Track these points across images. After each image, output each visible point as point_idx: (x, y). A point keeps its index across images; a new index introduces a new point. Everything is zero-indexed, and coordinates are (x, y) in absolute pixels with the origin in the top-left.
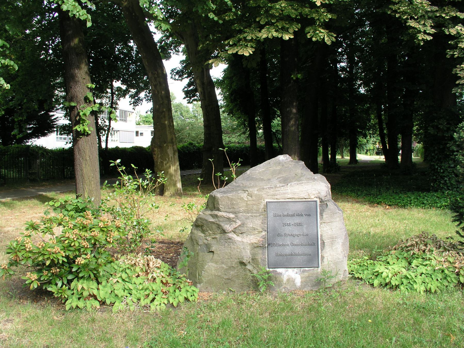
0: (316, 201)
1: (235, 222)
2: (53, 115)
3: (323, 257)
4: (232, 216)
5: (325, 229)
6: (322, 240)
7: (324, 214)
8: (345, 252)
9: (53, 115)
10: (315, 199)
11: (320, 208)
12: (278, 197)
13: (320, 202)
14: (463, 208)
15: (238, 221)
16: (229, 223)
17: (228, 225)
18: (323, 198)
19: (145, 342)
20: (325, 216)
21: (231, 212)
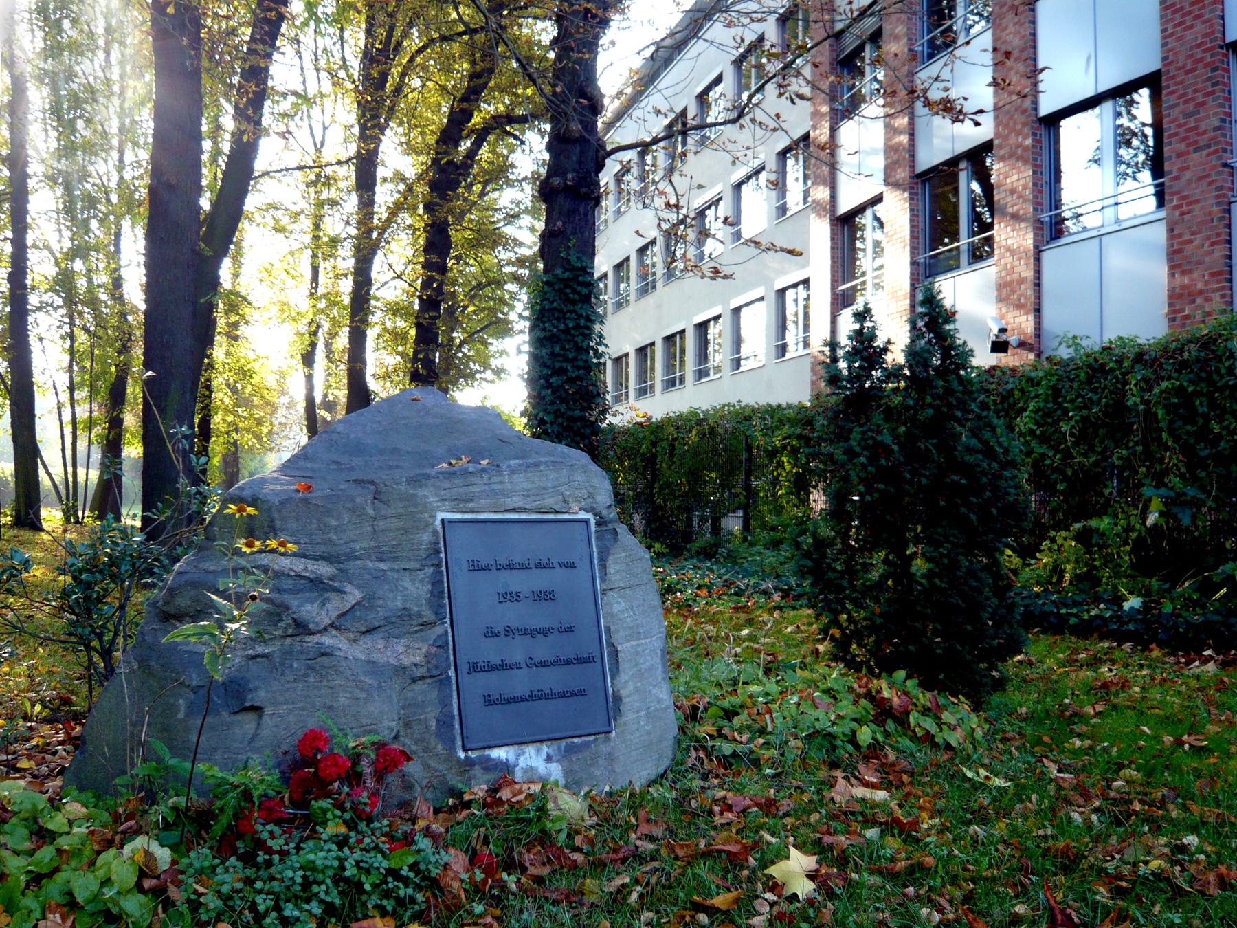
0: (586, 521)
4: (324, 569)
10: (582, 515)
13: (598, 524)
17: (316, 605)
18: (605, 513)
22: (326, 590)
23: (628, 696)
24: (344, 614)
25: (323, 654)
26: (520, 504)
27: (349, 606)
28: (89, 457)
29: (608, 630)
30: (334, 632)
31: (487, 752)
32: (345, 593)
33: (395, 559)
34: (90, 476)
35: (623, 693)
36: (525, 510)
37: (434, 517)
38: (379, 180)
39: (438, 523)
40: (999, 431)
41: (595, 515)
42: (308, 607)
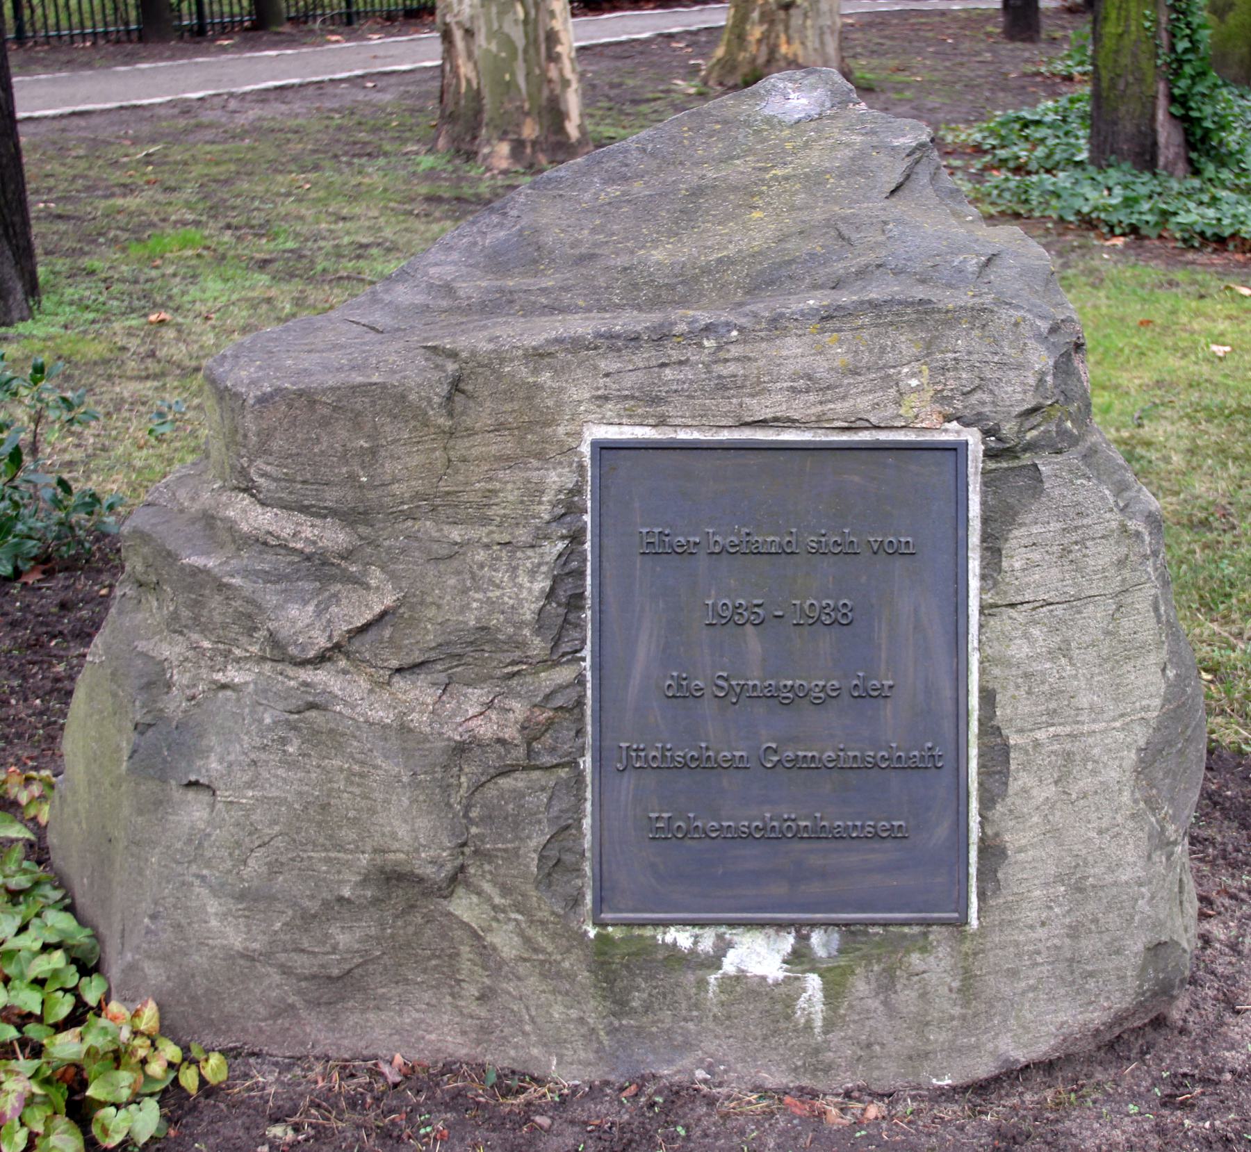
0: (956, 450)
1: (358, 582)
2: (469, 81)
3: (992, 852)
4: (334, 537)
5: (1019, 650)
6: (989, 729)
7: (1017, 537)
8: (1167, 809)
9: (469, 81)
10: (952, 433)
11: (984, 494)
12: (762, 408)
13: (990, 454)
14: (1181, 11)
15: (375, 576)
16: (319, 591)
17: (311, 608)
18: (1008, 428)
19: (1238, 651)
20: (1014, 561)
21: (333, 512)
22: (333, 579)
23: (1021, 850)
24: (363, 629)
25: (312, 706)
26: (781, 411)
27: (368, 616)
28: (957, 633)
29: (988, 697)
30: (343, 663)
31: (648, 932)
32: (367, 587)
33: (485, 520)
34: (254, 222)
35: (1010, 840)
36: (791, 423)
37: (578, 435)
38: (39, 251)
39: (586, 449)
40: (35, 332)
41: (987, 433)
42: (293, 611)
